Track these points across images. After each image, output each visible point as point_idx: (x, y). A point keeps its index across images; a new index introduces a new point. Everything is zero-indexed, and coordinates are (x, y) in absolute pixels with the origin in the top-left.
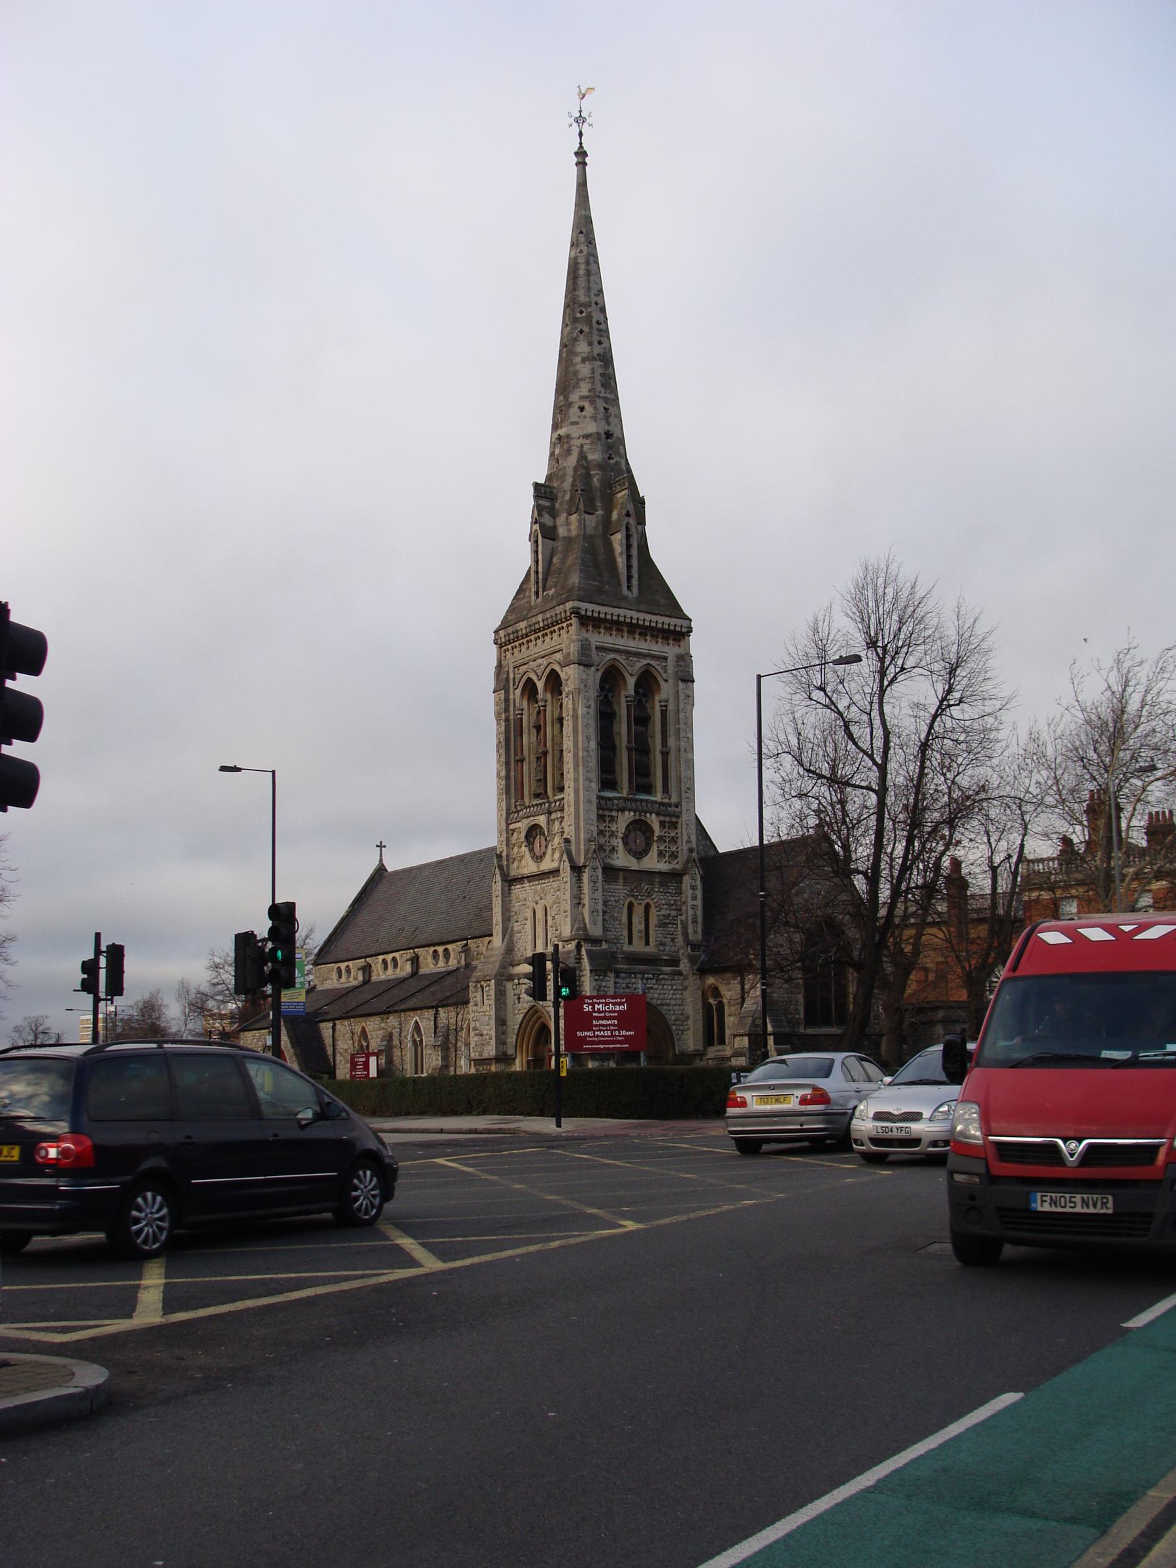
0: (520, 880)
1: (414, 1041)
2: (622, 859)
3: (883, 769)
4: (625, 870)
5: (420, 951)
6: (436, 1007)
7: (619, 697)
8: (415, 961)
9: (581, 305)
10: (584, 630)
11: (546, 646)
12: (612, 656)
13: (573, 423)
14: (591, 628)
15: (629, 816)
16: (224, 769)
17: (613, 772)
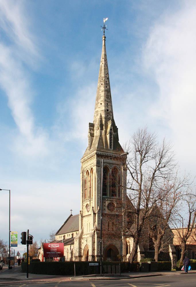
1: (67, 252)
2: (107, 211)
4: (109, 215)
5: (65, 234)
6: (71, 245)
7: (108, 174)
8: (73, 235)
9: (102, 77)
10: (98, 158)
12: (114, 165)
13: (99, 108)
14: (100, 157)
15: (109, 202)
17: (106, 191)
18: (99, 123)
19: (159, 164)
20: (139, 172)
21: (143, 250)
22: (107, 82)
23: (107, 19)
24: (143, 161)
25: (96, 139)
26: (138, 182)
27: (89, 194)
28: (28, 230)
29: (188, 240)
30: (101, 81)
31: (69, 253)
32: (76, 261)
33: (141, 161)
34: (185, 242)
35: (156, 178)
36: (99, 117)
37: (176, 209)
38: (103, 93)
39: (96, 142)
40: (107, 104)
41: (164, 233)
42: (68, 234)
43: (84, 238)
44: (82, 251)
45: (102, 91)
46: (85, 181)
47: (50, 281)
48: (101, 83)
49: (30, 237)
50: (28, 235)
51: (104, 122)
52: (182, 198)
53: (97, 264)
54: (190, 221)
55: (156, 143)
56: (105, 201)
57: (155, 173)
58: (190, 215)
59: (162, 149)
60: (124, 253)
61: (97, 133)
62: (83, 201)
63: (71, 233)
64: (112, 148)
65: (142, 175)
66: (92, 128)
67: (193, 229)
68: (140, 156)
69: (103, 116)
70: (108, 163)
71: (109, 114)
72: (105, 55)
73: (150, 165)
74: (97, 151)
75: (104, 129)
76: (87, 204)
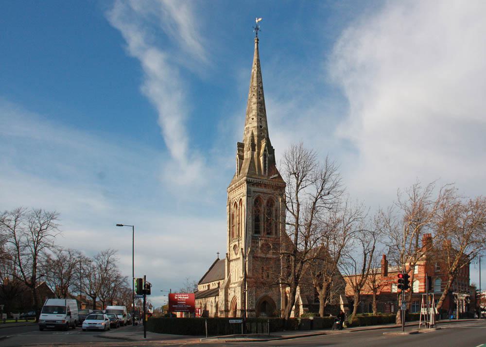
0: (232, 260)
2: (260, 254)
3: (297, 219)
8: (219, 284)
11: (238, 192)
12: (270, 196)
16: (118, 225)
18: (250, 143)
19: (321, 191)
20: (295, 201)
21: (307, 303)
22: (261, 93)
23: (260, 19)
24: (300, 187)
25: (246, 162)
26: (293, 214)
27: (237, 233)
28: (145, 276)
29: (363, 288)
30: (252, 91)
31: (212, 306)
32: (222, 317)
33: (298, 186)
34: (359, 291)
35: (318, 208)
36: (250, 135)
37: (346, 249)
38: (256, 105)
39: (247, 165)
40: (261, 119)
41: (332, 281)
42: (214, 283)
43: (231, 288)
44: (229, 304)
45: (254, 104)
46: (233, 215)
47: (173, 343)
48: (253, 93)
49: (147, 285)
50: (145, 283)
51: (256, 141)
52: (353, 235)
53: (240, 321)
54: (365, 265)
55: (316, 162)
56: (258, 241)
57: (316, 202)
58: (365, 258)
59: (324, 171)
60: (282, 306)
61: (247, 155)
62: (230, 240)
63: (217, 282)
64: (267, 174)
65: (298, 205)
66: (242, 149)
67: (369, 276)
68: (296, 180)
69: (256, 133)
70: (261, 193)
71: (263, 131)
72: (258, 60)
73: (307, 193)
74: (247, 177)
75: (256, 150)
76: (235, 245)
